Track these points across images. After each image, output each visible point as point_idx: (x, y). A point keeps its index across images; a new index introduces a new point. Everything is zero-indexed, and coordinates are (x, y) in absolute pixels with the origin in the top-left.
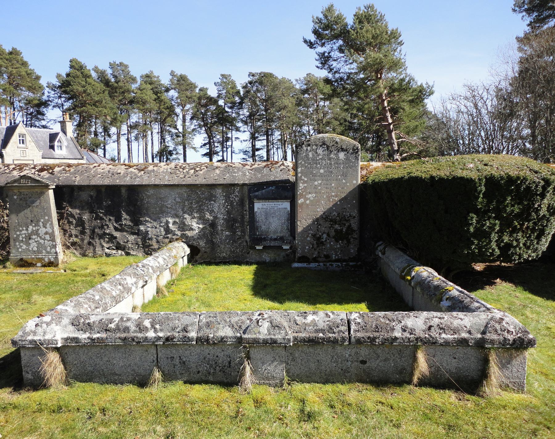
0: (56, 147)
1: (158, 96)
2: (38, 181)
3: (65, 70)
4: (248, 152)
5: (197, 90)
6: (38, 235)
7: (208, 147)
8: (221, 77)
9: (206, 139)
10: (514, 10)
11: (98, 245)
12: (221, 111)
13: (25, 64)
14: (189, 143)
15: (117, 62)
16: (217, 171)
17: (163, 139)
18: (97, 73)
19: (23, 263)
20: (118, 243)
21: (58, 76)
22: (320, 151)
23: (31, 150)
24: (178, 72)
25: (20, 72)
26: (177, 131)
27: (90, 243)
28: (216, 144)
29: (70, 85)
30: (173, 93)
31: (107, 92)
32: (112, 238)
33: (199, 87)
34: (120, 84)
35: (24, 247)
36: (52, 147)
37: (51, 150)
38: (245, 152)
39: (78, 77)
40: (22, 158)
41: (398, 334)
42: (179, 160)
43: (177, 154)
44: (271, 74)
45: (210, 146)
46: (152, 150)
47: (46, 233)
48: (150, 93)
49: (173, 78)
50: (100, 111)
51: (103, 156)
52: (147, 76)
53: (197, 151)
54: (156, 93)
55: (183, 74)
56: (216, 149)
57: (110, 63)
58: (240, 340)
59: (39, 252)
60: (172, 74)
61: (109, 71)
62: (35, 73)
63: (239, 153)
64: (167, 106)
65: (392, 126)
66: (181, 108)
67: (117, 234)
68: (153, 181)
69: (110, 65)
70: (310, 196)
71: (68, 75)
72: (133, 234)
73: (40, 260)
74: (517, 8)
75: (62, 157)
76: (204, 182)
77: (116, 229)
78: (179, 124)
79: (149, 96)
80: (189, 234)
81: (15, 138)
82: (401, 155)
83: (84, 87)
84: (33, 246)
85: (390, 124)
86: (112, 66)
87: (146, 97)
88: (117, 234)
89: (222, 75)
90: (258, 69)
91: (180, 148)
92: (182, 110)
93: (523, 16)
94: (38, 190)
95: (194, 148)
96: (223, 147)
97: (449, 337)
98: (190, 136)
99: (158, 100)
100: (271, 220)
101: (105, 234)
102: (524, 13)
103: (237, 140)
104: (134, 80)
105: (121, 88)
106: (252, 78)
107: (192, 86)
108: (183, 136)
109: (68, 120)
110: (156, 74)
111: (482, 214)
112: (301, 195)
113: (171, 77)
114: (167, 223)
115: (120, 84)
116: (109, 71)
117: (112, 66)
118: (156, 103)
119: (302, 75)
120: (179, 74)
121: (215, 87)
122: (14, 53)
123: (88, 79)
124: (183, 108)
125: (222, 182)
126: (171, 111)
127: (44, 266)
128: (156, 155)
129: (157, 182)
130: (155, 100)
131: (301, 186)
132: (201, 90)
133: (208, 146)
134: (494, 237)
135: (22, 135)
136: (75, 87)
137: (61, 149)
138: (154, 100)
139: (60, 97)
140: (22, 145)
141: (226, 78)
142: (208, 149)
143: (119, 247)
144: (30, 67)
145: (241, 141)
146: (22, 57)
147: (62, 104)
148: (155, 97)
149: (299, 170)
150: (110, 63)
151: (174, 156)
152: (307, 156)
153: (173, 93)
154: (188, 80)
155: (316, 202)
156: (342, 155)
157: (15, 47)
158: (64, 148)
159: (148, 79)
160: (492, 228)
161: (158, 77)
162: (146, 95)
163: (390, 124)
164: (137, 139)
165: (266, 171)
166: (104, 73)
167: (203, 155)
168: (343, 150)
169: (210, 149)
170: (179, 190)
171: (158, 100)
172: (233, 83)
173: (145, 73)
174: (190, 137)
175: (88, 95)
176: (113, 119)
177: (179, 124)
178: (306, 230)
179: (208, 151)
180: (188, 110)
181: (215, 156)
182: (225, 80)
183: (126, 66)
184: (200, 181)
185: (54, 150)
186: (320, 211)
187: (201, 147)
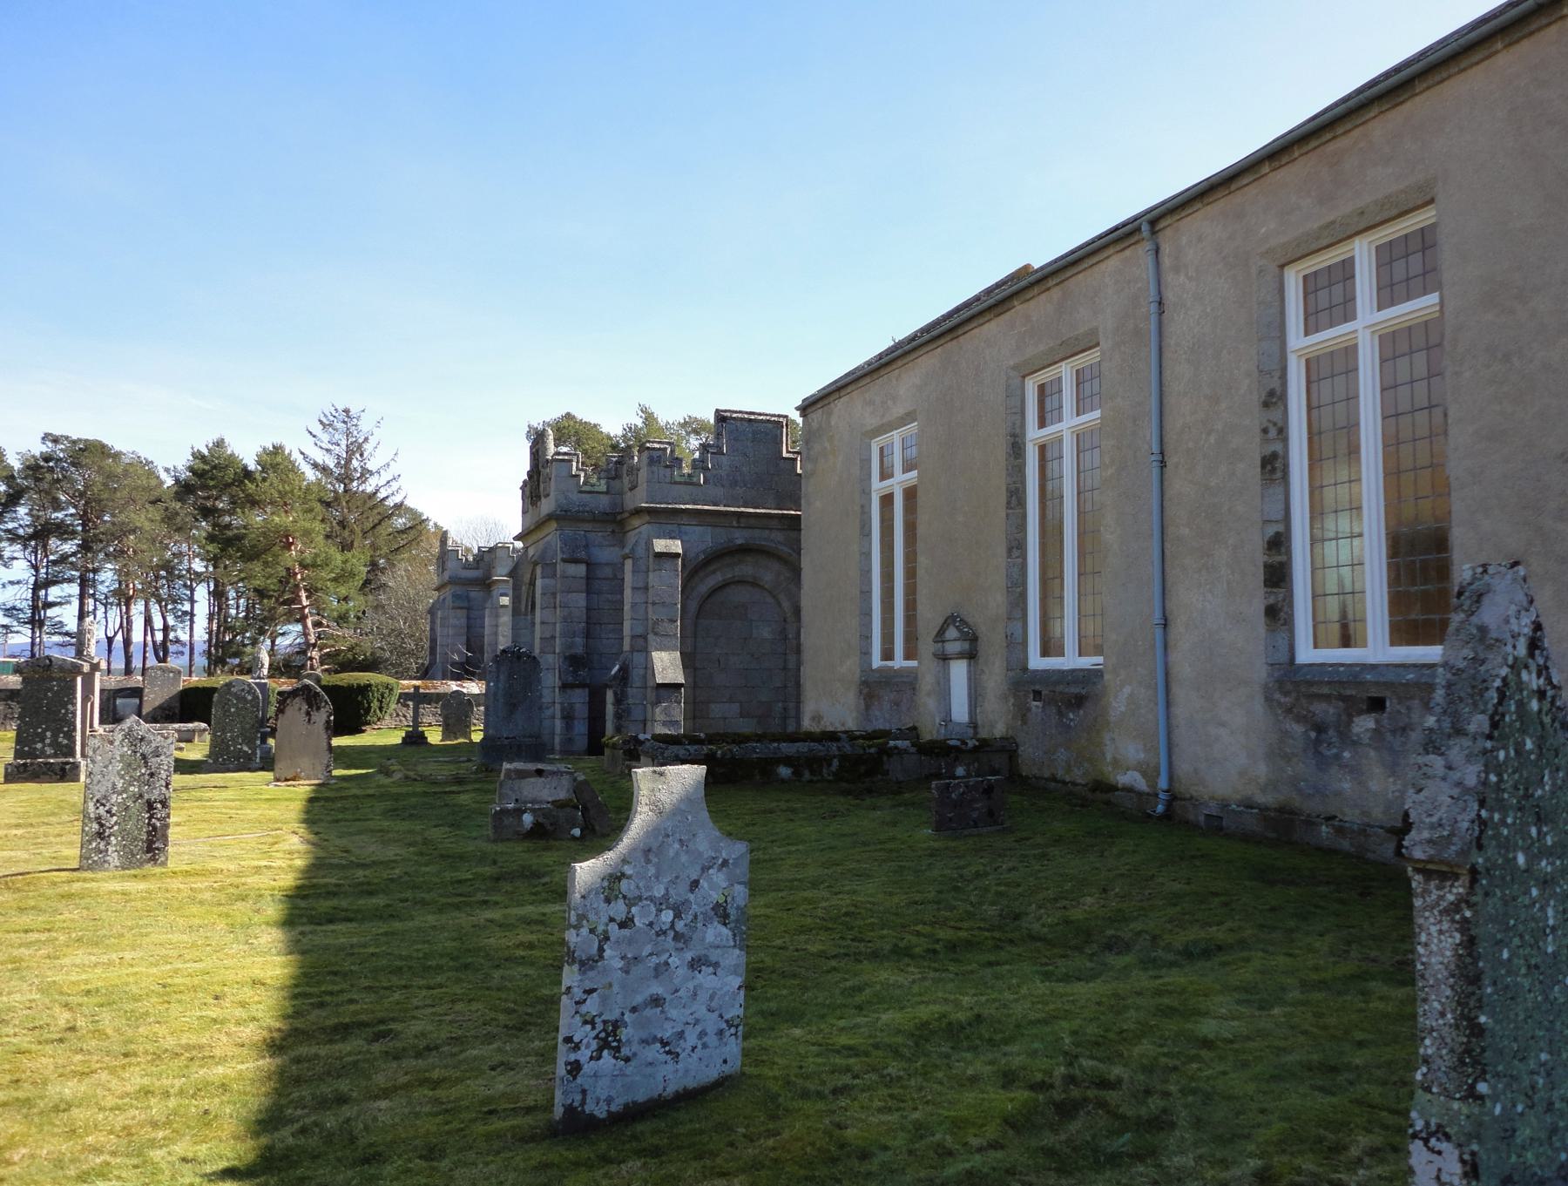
65: (307, 611)
82: (321, 650)
85: (304, 607)
106: (50, 444)
163: (304, 607)
186: (157, 704)
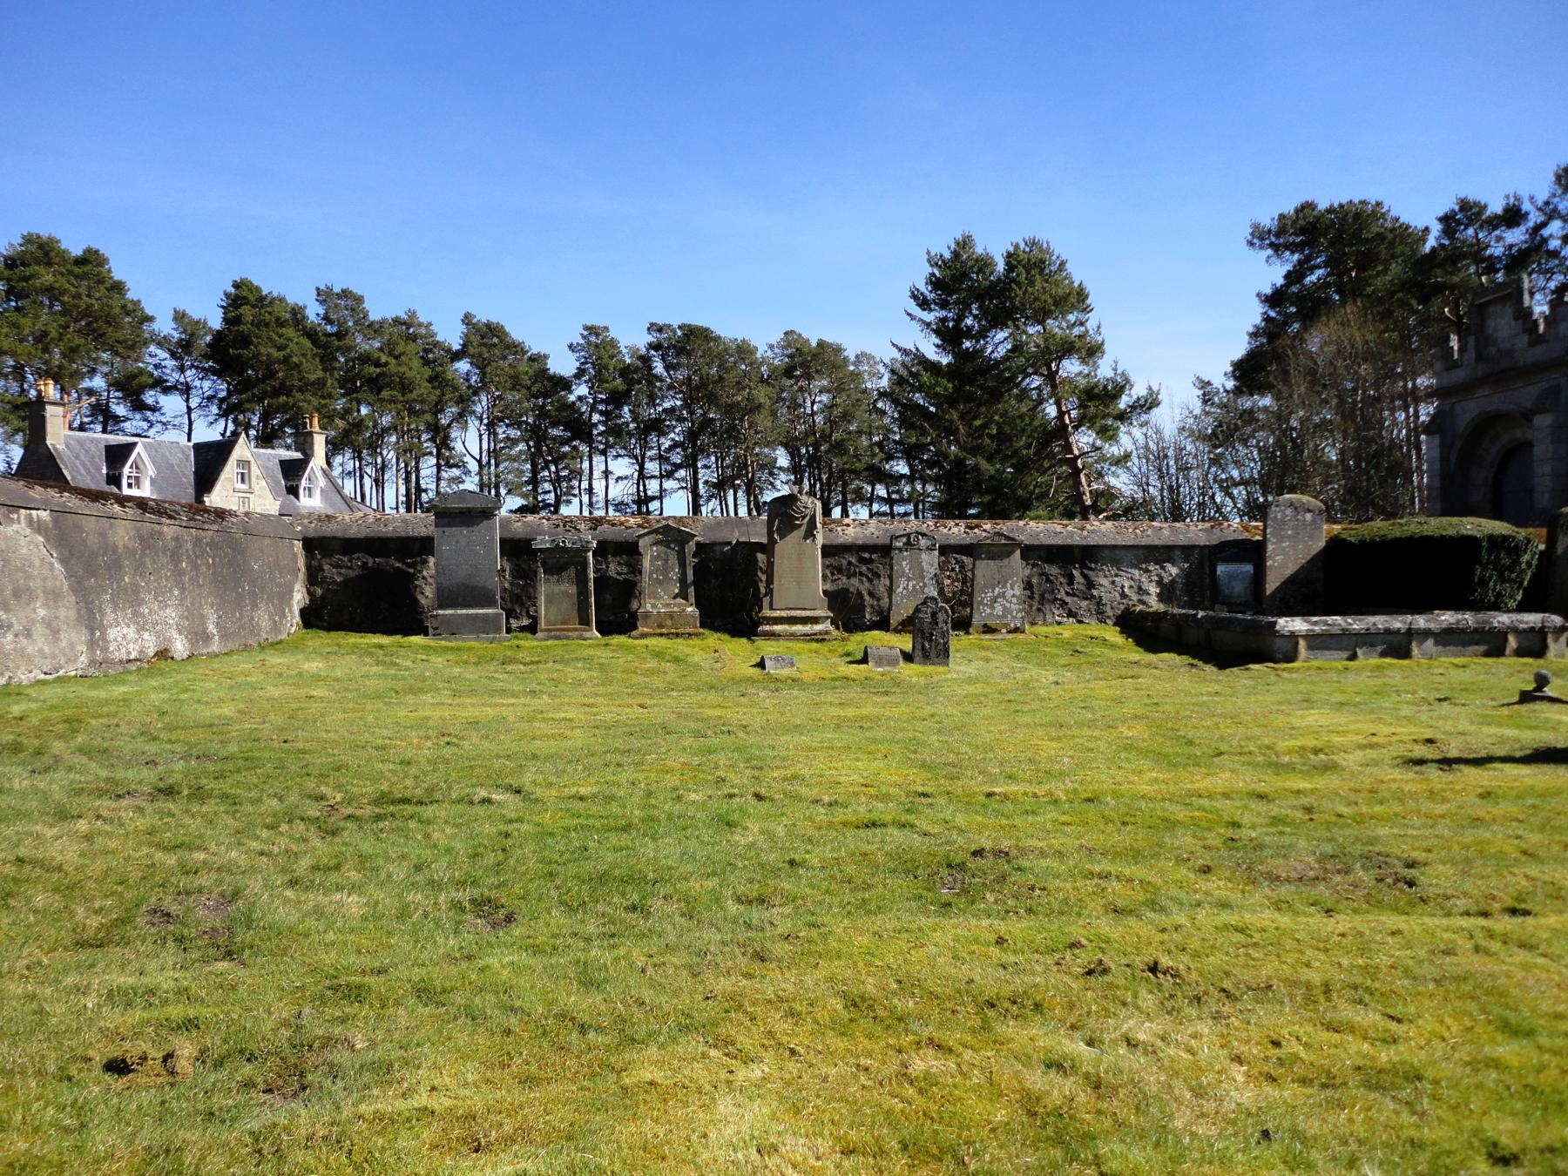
0: (301, 491)
2: (1012, 539)
6: (1004, 597)
10: (1251, 244)
11: (1048, 612)
13: (118, 287)
15: (337, 290)
19: (988, 630)
20: (1070, 610)
22: (1289, 511)
23: (260, 496)
24: (482, 316)
27: (1039, 610)
29: (251, 343)
32: (1064, 604)
35: (988, 611)
37: (292, 497)
41: (1496, 625)
44: (706, 330)
47: (1013, 596)
57: (318, 289)
59: (1004, 616)
60: (467, 319)
62: (142, 310)
67: (1068, 599)
69: (318, 295)
72: (1086, 599)
73: (1005, 625)
74: (1255, 241)
77: (1067, 594)
84: (998, 610)
85: (1076, 458)
86: (324, 296)
87: (409, 374)
88: (1068, 599)
89: (586, 328)
90: (676, 317)
93: (1269, 257)
94: (1009, 549)
97: (1525, 626)
100: (1234, 583)
101: (1056, 599)
102: (1270, 252)
109: (317, 429)
110: (423, 318)
111: (1485, 566)
114: (1123, 587)
119: (776, 337)
127: (1009, 632)
130: (431, 380)
131: (1270, 547)
134: (1491, 584)
135: (243, 463)
137: (310, 496)
140: (240, 486)
141: (597, 335)
143: (1071, 614)
144: (130, 295)
146: (109, 271)
149: (1268, 531)
150: (318, 289)
154: (507, 334)
155: (1283, 566)
156: (1308, 516)
158: (317, 493)
160: (1491, 577)
162: (411, 369)
168: (1310, 511)
170: (1135, 552)
175: (292, 369)
178: (1273, 593)
182: (593, 339)
183: (360, 300)
185: (297, 496)
186: (1288, 572)
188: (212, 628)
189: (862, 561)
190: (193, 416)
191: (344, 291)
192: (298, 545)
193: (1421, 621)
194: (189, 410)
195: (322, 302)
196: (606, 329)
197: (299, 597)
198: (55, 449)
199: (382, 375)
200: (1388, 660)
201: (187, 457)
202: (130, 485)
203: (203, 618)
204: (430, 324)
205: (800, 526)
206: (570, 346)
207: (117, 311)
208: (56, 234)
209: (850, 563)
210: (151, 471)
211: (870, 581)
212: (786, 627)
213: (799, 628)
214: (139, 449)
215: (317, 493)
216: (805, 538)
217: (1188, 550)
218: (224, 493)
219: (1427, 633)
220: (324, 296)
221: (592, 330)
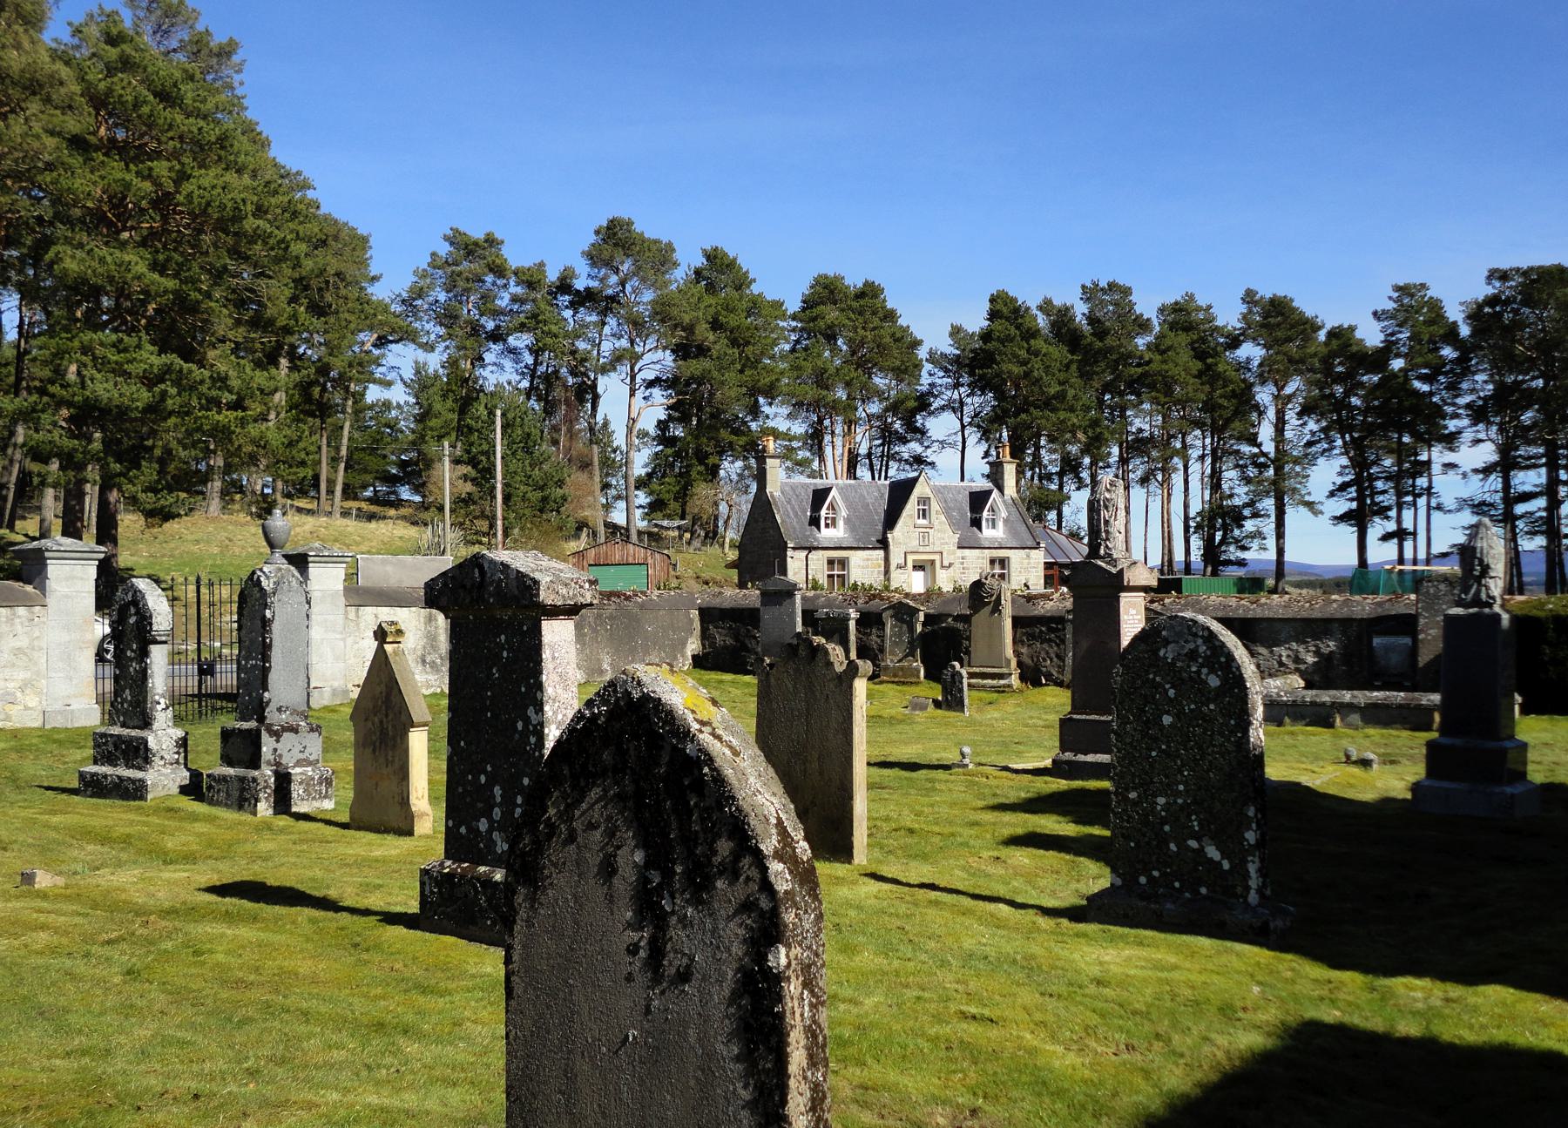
0: (984, 523)
1: (1206, 364)
3: (976, 321)
4: (1491, 505)
5: (1322, 336)
7: (1355, 494)
8: (1396, 295)
9: (1347, 471)
12: (1395, 386)
13: (891, 316)
14: (1294, 490)
15: (1103, 284)
16: (1335, 605)
17: (1215, 481)
18: (1048, 315)
21: (956, 331)
22: (1442, 587)
23: (939, 531)
24: (1266, 291)
25: (881, 337)
26: (1256, 450)
28: (1380, 485)
30: (1251, 352)
31: (1074, 367)
33: (1328, 327)
34: (1110, 341)
36: (976, 523)
38: (1480, 507)
39: (1012, 340)
40: (921, 549)
42: (1264, 538)
43: (1256, 515)
45: (1360, 491)
46: (1186, 506)
48: (1185, 356)
49: (1250, 311)
50: (1063, 422)
51: (1055, 528)
52: (1177, 308)
53: (1316, 513)
54: (1200, 355)
55: (1281, 293)
56: (1379, 498)
57: (1083, 287)
58: (1334, 703)
60: (1249, 297)
61: (1080, 309)
63: (1458, 510)
64: (1233, 391)
66: (1274, 390)
68: (1267, 614)
70: (1431, 631)
71: (986, 336)
75: (996, 545)
76: (1319, 615)
78: (1266, 432)
79: (1183, 362)
80: (1302, 667)
81: (911, 507)
83: (1024, 363)
86: (1090, 293)
89: (1398, 288)
91: (1268, 504)
92: (1276, 397)
95: (1310, 505)
96: (1400, 494)
98: (1298, 469)
99: (1209, 375)
103: (1451, 473)
104: (1143, 325)
105: (1110, 350)
106: (1498, 284)
107: (1307, 326)
108: (1278, 470)
109: (1008, 458)
110: (1202, 301)
112: (1422, 631)
113: (1244, 309)
114: (1280, 656)
115: (1110, 341)
116: (1080, 309)
117: (1090, 293)
118: (1202, 384)
120: (1268, 295)
121: (1375, 323)
122: (870, 292)
123: (1032, 342)
124: (1279, 391)
125: (1338, 616)
126: (1245, 404)
128: (1199, 527)
129: (1271, 615)
130: (1200, 375)
131: (1422, 621)
132: (1332, 334)
133: (1353, 490)
135: (924, 501)
136: (1004, 367)
138: (1195, 377)
139: (957, 386)
140: (922, 522)
141: (1412, 296)
142: (1352, 500)
144: (902, 322)
145: (1465, 475)
147: (961, 399)
148: (1199, 365)
151: (1249, 526)
152: (1428, 592)
153: (1251, 352)
157: (871, 279)
158: (1000, 524)
159: (1182, 317)
161: (1210, 307)
164: (1144, 481)
165: (1387, 605)
166: (1065, 315)
167: (1335, 518)
169: (1360, 499)
171: (1209, 375)
172: (1435, 307)
173: (1173, 301)
174: (1298, 474)
175: (1033, 384)
176: (1091, 438)
177: (1266, 432)
179: (1354, 505)
180: (1289, 398)
181: (1377, 519)
183: (1127, 291)
184: (1316, 615)
185: (980, 528)
187: (1332, 494)
188: (605, 666)
189: (1051, 630)
190: (966, 432)
191: (1110, 285)
192: (695, 614)
193: (1347, 696)
194: (963, 427)
195: (1088, 300)
196: (1423, 286)
197: (693, 646)
198: (772, 496)
199: (1145, 375)
200: (1309, 728)
201: (882, 496)
202: (827, 526)
203: (599, 661)
204: (1210, 307)
205: (989, 603)
206: (1375, 314)
207: (888, 340)
208: (841, 271)
209: (1041, 631)
210: (844, 512)
211: (1058, 645)
212: (990, 681)
213: (989, 682)
214: (834, 492)
215: (1000, 524)
216: (993, 612)
217: (1346, 622)
218: (906, 529)
219: (1351, 707)
220: (1090, 293)
221: (1403, 290)
